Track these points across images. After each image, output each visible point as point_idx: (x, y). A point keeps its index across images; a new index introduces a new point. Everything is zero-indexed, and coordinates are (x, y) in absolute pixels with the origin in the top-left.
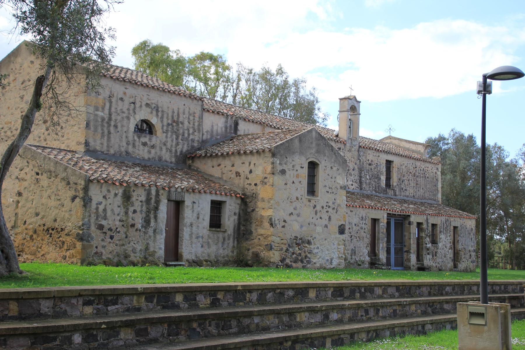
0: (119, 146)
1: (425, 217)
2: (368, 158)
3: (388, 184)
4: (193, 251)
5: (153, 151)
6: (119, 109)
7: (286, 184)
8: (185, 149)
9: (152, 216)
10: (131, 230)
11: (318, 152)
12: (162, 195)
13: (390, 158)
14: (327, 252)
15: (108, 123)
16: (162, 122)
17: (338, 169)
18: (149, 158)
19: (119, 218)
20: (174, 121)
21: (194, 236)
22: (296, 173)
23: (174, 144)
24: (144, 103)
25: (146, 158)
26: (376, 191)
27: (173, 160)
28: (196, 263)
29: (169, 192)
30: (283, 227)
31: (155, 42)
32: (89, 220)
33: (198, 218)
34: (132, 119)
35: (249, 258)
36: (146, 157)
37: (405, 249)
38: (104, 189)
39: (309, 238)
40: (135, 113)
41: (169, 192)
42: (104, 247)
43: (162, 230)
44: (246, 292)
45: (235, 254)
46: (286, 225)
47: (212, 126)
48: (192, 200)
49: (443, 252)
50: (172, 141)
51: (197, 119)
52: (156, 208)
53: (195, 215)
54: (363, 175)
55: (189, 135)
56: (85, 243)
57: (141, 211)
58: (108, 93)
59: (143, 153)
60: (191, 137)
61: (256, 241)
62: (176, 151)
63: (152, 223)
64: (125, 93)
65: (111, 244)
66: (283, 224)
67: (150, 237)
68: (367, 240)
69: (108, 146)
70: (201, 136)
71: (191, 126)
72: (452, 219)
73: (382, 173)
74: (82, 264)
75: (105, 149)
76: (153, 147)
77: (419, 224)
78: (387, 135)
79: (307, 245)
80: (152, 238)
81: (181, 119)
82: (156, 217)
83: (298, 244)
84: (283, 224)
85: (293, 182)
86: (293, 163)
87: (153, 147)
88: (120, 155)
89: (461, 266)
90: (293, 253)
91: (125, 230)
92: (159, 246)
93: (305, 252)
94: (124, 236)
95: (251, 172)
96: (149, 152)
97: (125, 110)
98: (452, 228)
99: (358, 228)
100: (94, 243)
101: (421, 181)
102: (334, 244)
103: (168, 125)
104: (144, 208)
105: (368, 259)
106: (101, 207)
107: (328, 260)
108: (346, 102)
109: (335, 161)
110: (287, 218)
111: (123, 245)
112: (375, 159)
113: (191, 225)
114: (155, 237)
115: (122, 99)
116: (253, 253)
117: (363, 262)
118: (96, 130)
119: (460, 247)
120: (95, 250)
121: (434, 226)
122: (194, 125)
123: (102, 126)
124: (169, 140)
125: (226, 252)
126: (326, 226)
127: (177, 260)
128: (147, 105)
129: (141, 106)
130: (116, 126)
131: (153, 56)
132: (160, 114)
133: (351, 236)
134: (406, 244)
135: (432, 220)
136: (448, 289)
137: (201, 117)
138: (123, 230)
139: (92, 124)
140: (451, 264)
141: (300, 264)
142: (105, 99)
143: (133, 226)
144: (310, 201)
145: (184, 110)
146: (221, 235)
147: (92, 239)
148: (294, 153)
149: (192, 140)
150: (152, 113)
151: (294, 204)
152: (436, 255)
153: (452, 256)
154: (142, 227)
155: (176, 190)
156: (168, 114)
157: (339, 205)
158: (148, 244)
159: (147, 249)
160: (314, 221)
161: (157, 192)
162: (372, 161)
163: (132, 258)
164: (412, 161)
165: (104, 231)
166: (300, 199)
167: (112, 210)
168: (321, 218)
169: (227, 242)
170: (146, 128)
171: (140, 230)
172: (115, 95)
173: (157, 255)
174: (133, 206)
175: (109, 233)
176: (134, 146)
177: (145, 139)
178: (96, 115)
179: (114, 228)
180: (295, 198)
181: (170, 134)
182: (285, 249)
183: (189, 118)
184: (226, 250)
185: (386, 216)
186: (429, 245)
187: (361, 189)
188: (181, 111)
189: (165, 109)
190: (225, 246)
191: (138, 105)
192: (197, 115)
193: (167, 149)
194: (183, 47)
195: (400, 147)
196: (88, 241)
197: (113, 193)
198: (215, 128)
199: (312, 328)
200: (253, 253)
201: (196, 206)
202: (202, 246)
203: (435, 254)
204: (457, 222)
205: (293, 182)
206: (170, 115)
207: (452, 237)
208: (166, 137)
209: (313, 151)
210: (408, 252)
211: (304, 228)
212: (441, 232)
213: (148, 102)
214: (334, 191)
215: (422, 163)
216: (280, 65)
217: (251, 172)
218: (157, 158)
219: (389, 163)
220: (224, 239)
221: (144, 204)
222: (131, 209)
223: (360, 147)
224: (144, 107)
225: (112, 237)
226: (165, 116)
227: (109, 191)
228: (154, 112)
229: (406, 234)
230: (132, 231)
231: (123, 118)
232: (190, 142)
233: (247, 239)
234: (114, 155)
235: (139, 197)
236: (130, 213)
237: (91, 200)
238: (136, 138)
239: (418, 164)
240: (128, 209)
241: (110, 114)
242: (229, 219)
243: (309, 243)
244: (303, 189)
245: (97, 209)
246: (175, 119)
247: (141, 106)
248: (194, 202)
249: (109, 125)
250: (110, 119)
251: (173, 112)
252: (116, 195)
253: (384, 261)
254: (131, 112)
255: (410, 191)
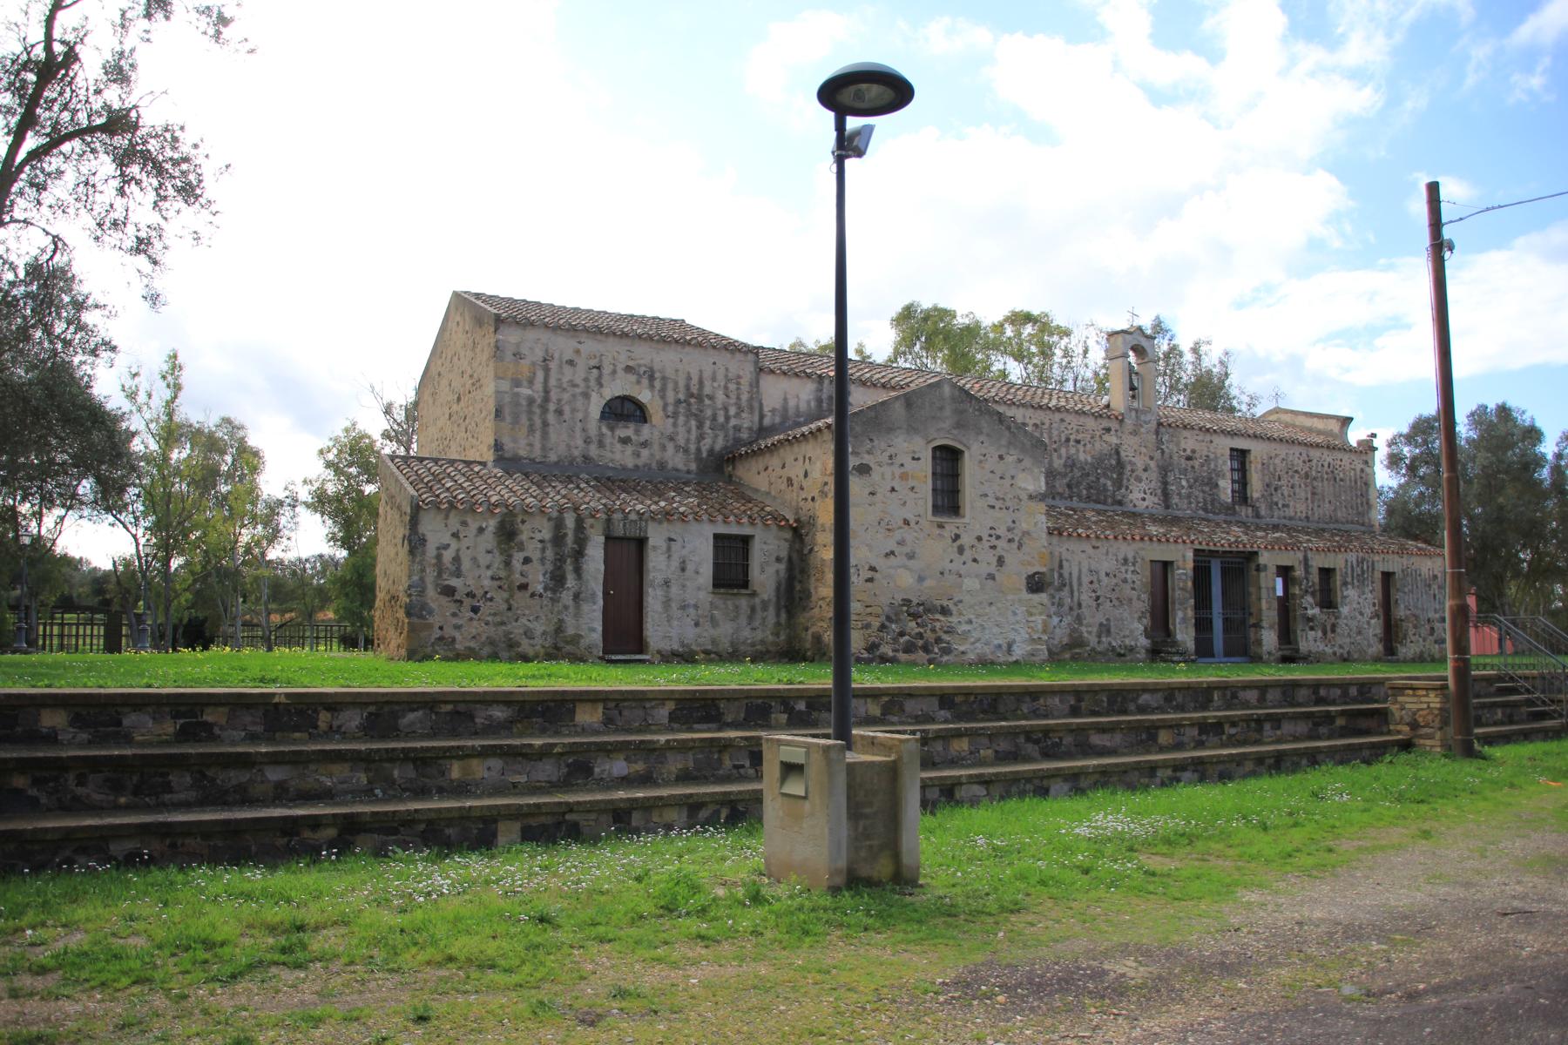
0: (568, 446)
1: (1300, 555)
2: (1183, 446)
3: (1242, 495)
4: (674, 633)
5: (645, 453)
6: (565, 380)
7: (872, 494)
8: (720, 444)
9: (569, 567)
10: (518, 595)
11: (959, 425)
12: (592, 526)
13: (1241, 444)
14: (996, 630)
15: (541, 406)
16: (663, 397)
17: (1020, 461)
18: (637, 466)
19: (489, 573)
20: (692, 395)
21: (674, 605)
22: (898, 471)
23: (693, 437)
24: (620, 367)
25: (630, 465)
26: (1205, 510)
27: (693, 466)
28: (684, 657)
29: (609, 521)
30: (870, 580)
31: (926, 304)
32: (422, 579)
33: (683, 570)
34: (594, 396)
35: (808, 645)
36: (630, 462)
37: (1252, 621)
38: (454, 522)
39: (945, 603)
40: (601, 385)
41: (609, 521)
42: (457, 627)
43: (594, 595)
44: (315, 711)
45: (783, 637)
46: (877, 576)
47: (785, 400)
48: (667, 535)
49: (1353, 624)
50: (689, 432)
51: (745, 387)
52: (579, 554)
53: (675, 563)
54: (1171, 478)
55: (727, 418)
56: (415, 620)
57: (542, 560)
58: (539, 354)
59: (622, 457)
60: (733, 422)
61: (816, 610)
62: (699, 450)
63: (571, 581)
64: (578, 352)
65: (475, 623)
66: (870, 574)
67: (566, 607)
68: (1142, 603)
69: (544, 448)
70: (756, 418)
71: (733, 401)
72: (1376, 558)
73: (1220, 474)
74: (409, 658)
75: (537, 453)
76: (645, 444)
77: (1285, 572)
78: (1272, 406)
79: (938, 616)
80: (571, 610)
81: (707, 390)
82: (578, 571)
83: (915, 616)
84: (870, 574)
85: (893, 489)
86: (891, 451)
87: (645, 444)
88: (571, 463)
89: (1407, 650)
90: (902, 634)
91: (506, 595)
92: (590, 623)
93: (933, 630)
94: (505, 606)
95: (806, 475)
96: (638, 455)
97: (578, 381)
98: (1378, 576)
99: (1114, 581)
100: (435, 620)
101: (1325, 488)
102: (1015, 614)
103: (679, 402)
104: (549, 554)
105: (1144, 642)
106: (448, 556)
107: (1000, 646)
108: (1120, 338)
109: (1010, 443)
110: (880, 563)
111: (503, 623)
112: (1202, 449)
113: (667, 583)
114: (578, 607)
115: (571, 363)
116: (813, 635)
117: (1132, 649)
118: (516, 420)
119: (1400, 612)
120: (437, 633)
121: (1326, 573)
122: (738, 398)
123: (530, 412)
124: (681, 430)
125: (759, 635)
126: (991, 577)
127: (641, 652)
128: (629, 369)
129: (614, 372)
130: (559, 412)
131: (922, 326)
132: (658, 384)
133: (1098, 598)
134: (1253, 610)
135: (1318, 561)
136: (1145, 698)
137: (755, 384)
138: (499, 597)
139: (507, 411)
140: (1377, 648)
141: (921, 656)
142: (534, 364)
143: (523, 587)
144: (941, 526)
145: (714, 373)
146: (744, 603)
147: (431, 612)
148: (890, 430)
149: (735, 427)
150: (638, 382)
151: (898, 535)
152: (1333, 631)
153: (1379, 631)
154: (546, 589)
155: (626, 518)
156: (676, 383)
157: (1026, 533)
158: (561, 621)
159: (559, 629)
160: (955, 566)
161: (579, 522)
162: (1193, 451)
163: (525, 646)
164: (1297, 449)
165: (457, 597)
166: (912, 524)
167: (474, 559)
168: (975, 560)
169: (759, 614)
170: (624, 411)
171: (541, 596)
172: (556, 355)
173: (584, 643)
174: (521, 548)
175: (468, 602)
176: (601, 444)
177: (627, 431)
178: (517, 394)
179: (479, 593)
180: (901, 523)
181: (681, 419)
182: (876, 624)
183: (726, 388)
184: (764, 630)
185: (1190, 555)
186: (1314, 611)
187: (1167, 507)
188: (707, 375)
189: (669, 373)
190: (757, 623)
191: (607, 370)
192: (745, 382)
193: (678, 448)
194: (980, 303)
195: (1294, 426)
196: (421, 617)
197: (473, 526)
198: (792, 403)
199: (522, 794)
200: (813, 635)
201: (675, 547)
202: (697, 625)
203: (1329, 630)
204: (1394, 564)
205: (893, 489)
206: (682, 384)
207: (1379, 593)
208: (675, 425)
209: (947, 425)
210: (1258, 626)
211: (928, 583)
212: (1345, 584)
213: (631, 363)
214: (1008, 504)
215: (1326, 452)
216: (1158, 318)
217: (806, 475)
218: (654, 466)
219: (1240, 456)
220: (753, 609)
221: (549, 545)
222: (518, 557)
223: (1160, 424)
224: (620, 373)
225: (475, 610)
226: (670, 386)
227: (464, 523)
228: (645, 381)
229: (1252, 590)
230: (521, 599)
231: (574, 396)
232: (731, 432)
233: (804, 609)
234: (556, 463)
235: (535, 534)
236: (517, 562)
237: (423, 541)
238: (604, 430)
239: (1315, 454)
240: (510, 556)
241: (547, 391)
242: (765, 572)
243: (945, 611)
244: (921, 502)
245: (439, 557)
246: (694, 390)
247: (614, 372)
248: (671, 540)
249: (545, 410)
250: (546, 399)
251: (689, 378)
252: (481, 530)
253: (1190, 645)
254: (593, 383)
255: (1299, 508)
